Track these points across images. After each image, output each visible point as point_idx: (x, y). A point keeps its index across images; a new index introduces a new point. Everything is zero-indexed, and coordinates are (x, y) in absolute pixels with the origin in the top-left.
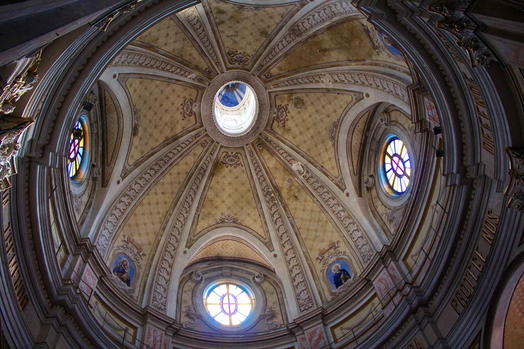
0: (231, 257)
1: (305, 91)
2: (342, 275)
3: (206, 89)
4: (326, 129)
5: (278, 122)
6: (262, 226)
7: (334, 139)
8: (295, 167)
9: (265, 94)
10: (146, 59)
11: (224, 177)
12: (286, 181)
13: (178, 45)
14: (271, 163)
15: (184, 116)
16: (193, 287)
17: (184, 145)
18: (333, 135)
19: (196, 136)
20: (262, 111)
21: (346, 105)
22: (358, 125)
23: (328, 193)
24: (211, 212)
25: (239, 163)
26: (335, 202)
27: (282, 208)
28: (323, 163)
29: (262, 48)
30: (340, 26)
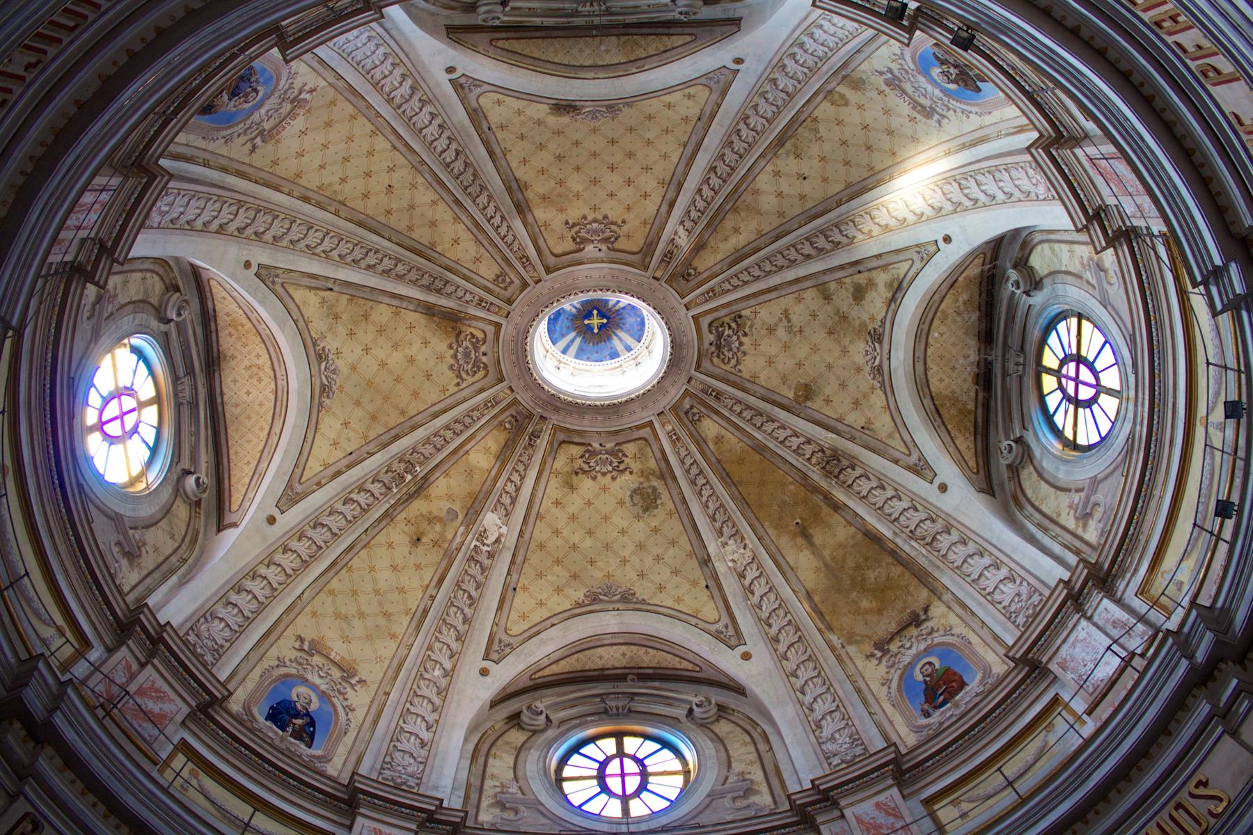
0: (222, 394)
1: (681, 508)
2: (299, 722)
3: (643, 273)
4: (609, 576)
5: (581, 457)
6: (327, 466)
7: (594, 601)
8: (491, 520)
9: (644, 414)
10: (756, 131)
12: (448, 505)
13: (768, 202)
14: (481, 457)
17: (503, 230)
18: (601, 597)
21: (689, 612)
24: (339, 320)
25: (464, 375)
27: (384, 509)
28: (525, 588)
29: (763, 391)
30: (890, 560)
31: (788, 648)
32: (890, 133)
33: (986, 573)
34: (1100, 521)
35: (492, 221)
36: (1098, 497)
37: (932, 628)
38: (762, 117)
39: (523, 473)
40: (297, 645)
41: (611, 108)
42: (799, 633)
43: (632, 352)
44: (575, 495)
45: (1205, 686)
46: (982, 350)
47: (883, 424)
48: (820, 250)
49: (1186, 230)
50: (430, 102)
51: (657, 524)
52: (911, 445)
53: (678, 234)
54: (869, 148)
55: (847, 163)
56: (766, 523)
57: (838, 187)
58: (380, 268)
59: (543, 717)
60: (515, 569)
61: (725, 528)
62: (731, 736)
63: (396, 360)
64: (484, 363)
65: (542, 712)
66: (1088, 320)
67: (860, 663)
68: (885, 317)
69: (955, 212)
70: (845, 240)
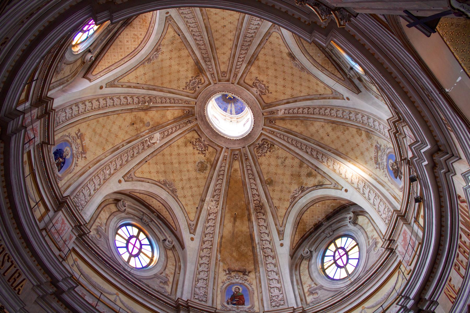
0: (120, 34)
2: (61, 160)
4: (174, 180)
7: (164, 184)
8: (157, 135)
9: (223, 144)
10: (331, 114)
13: (313, 129)
14: (170, 114)
15: (258, 80)
17: (239, 63)
18: (167, 185)
19: (236, 75)
20: (212, 132)
21: (187, 211)
24: (172, 45)
25: (188, 88)
28: (149, 164)
29: (259, 170)
30: (251, 248)
31: (206, 248)
32: (362, 154)
34: (314, 298)
35: (239, 59)
36: (319, 292)
37: (247, 279)
38: (336, 114)
39: (177, 129)
40: (77, 132)
41: (303, 69)
42: (211, 247)
43: (231, 115)
47: (282, 212)
49: (412, 284)
51: (199, 177)
52: (284, 225)
53: (281, 110)
54: (352, 149)
55: (343, 145)
56: (228, 206)
58: (198, 42)
59: (125, 208)
60: (151, 155)
61: (216, 197)
62: (171, 258)
64: (196, 90)
65: (125, 206)
66: (359, 248)
67: (221, 270)
68: (310, 188)
69: (356, 189)
70: (321, 160)
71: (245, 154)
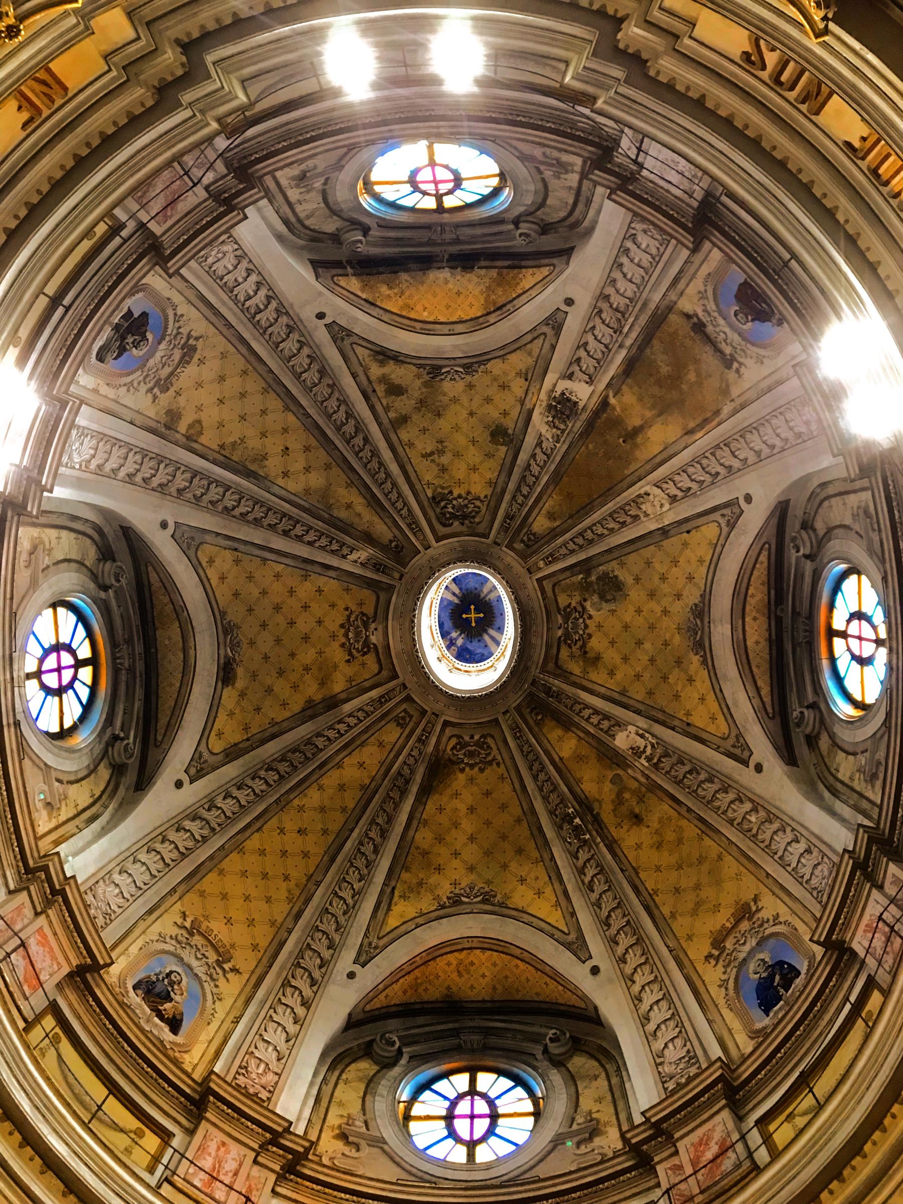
0: (483, 1001)
1: (616, 554)
2: (777, 978)
6: (558, 904)
8: (622, 741)
9: (530, 586)
10: (240, 499)
11: (457, 794)
13: (316, 480)
16: (372, 1073)
17: (352, 721)
19: (381, 700)
22: (750, 592)
23: (710, 780)
25: (490, 758)
26: (731, 796)
27: (604, 850)
28: (688, 714)
31: (736, 457)
33: (636, 261)
42: (722, 445)
44: (605, 656)
45: (647, 61)
46: (441, 264)
48: (358, 429)
50: (212, 801)
52: (536, 334)
57: (291, 418)
58: (378, 840)
63: (468, 825)
67: (746, 385)
68: (415, 365)
71: (504, 528)
